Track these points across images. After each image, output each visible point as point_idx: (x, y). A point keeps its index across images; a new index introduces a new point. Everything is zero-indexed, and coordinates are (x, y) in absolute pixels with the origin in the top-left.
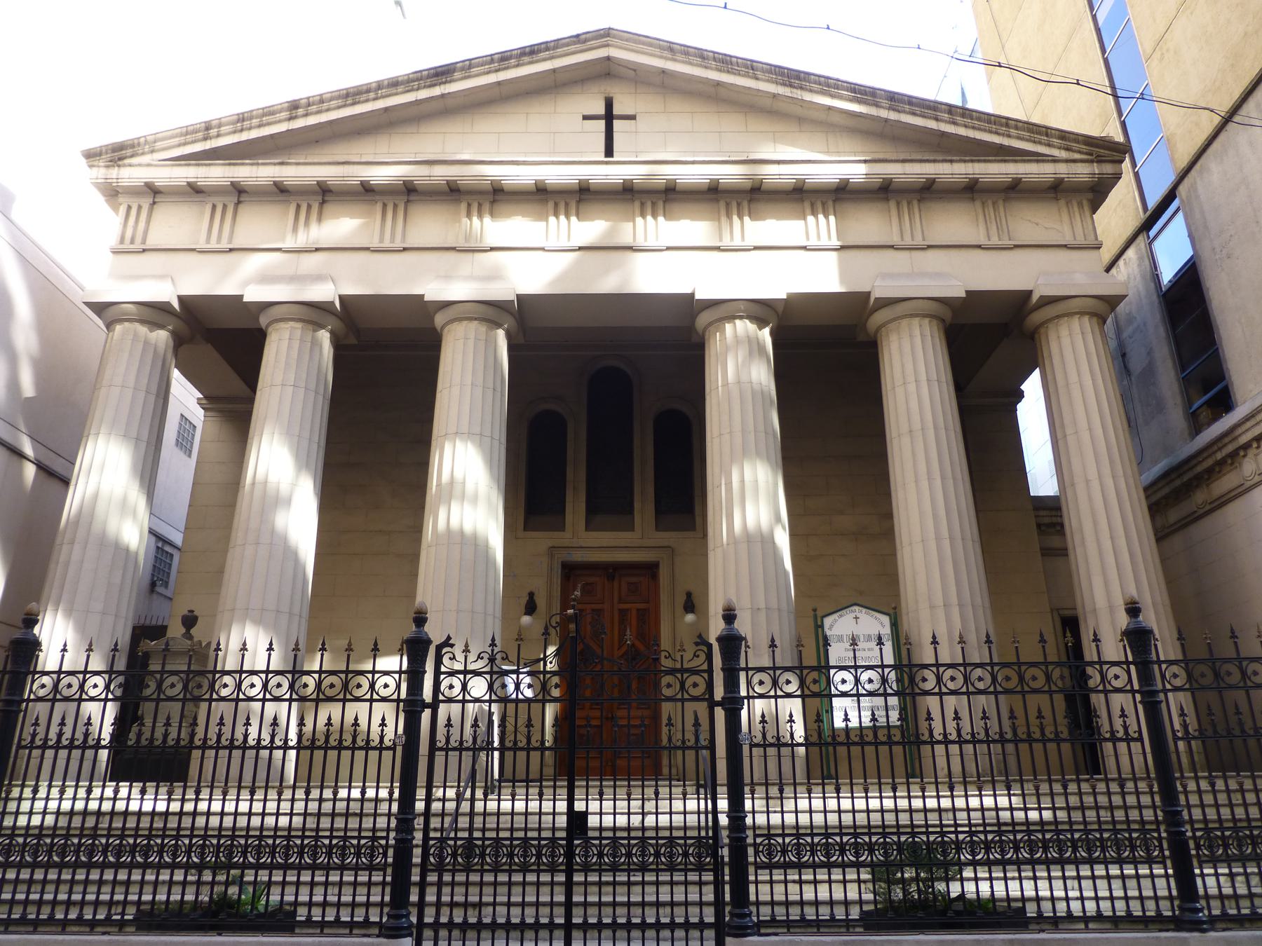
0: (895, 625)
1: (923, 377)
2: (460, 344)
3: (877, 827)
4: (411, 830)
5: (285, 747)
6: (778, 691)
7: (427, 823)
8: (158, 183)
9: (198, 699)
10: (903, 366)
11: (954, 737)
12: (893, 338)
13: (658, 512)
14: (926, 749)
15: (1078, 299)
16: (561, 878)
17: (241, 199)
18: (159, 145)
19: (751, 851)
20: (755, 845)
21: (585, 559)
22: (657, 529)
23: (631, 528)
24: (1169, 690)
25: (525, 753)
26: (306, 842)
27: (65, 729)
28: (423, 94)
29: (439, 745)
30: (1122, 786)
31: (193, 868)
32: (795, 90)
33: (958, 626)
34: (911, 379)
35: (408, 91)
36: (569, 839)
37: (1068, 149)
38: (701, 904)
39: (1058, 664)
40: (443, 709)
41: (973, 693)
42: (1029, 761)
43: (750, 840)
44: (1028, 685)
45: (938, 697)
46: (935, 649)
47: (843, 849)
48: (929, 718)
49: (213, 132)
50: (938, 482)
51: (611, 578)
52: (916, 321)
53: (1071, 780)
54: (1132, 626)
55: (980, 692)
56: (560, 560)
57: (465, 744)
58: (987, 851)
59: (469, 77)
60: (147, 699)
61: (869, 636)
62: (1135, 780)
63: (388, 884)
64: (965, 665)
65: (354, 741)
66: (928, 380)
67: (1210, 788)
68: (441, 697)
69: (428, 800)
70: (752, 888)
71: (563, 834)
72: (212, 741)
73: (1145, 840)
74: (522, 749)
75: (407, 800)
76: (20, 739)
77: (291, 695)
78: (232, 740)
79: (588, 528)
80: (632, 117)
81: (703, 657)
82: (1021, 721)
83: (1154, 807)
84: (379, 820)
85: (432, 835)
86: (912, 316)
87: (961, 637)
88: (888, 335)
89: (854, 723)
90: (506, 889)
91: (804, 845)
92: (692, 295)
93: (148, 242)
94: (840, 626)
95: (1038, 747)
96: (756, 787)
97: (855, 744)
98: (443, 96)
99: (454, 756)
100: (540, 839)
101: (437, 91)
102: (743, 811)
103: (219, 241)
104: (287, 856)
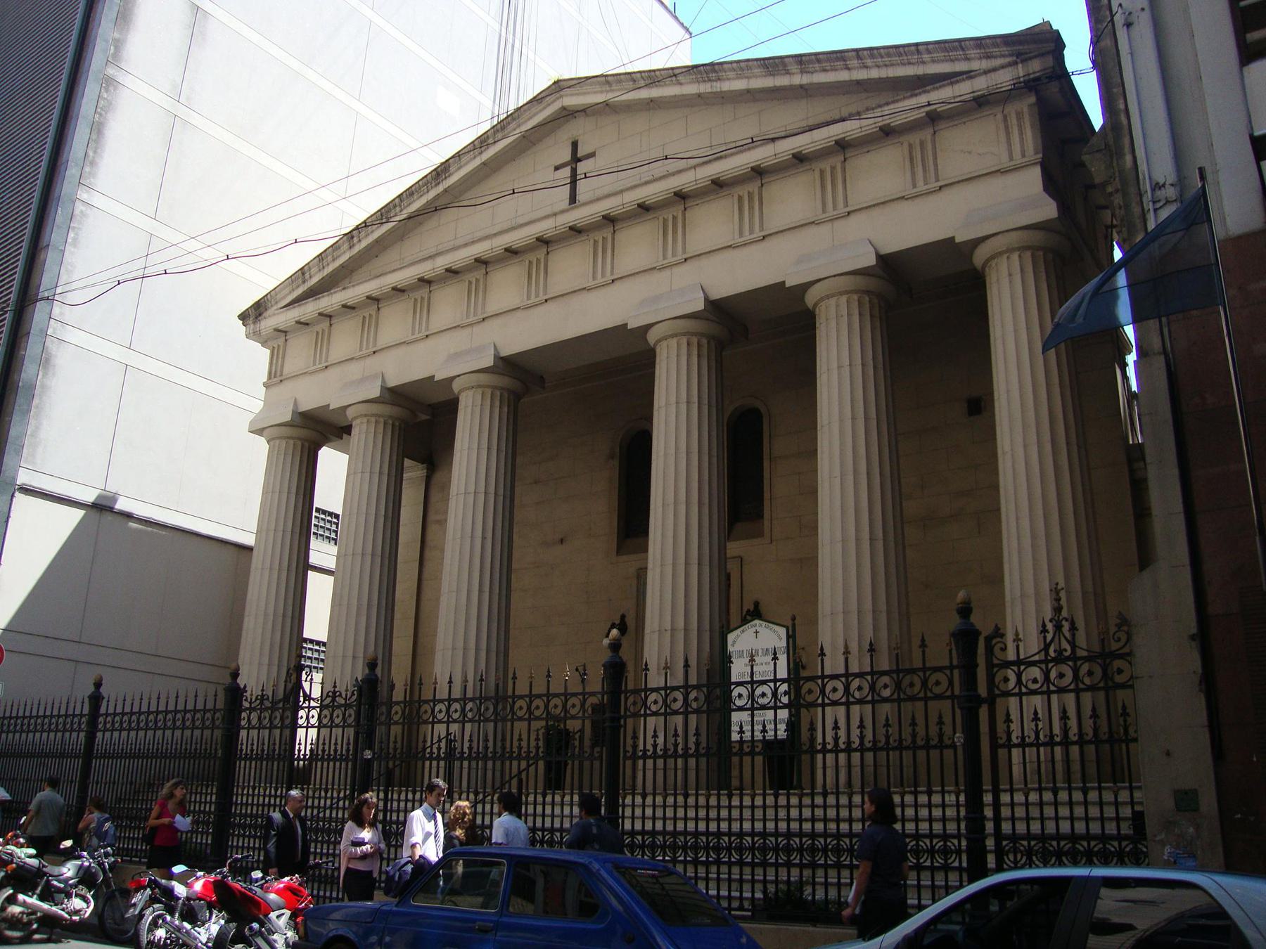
0: (791, 637)
2: (1005, 282)
5: (645, 757)
8: (328, 311)
9: (504, 720)
15: (999, 237)
17: (847, 156)
18: (279, 297)
24: (1054, 692)
27: (918, 729)
28: (432, 194)
32: (715, 84)
33: (869, 633)
35: (421, 196)
37: (989, 57)
39: (783, 681)
41: (1026, 694)
42: (750, 772)
48: (1008, 720)
49: (307, 276)
50: (695, 509)
53: (1093, 788)
55: (886, 700)
57: (904, 743)
59: (461, 167)
61: (767, 650)
62: (837, 794)
64: (752, 682)
65: (914, 741)
69: (997, 805)
72: (908, 741)
75: (975, 804)
76: (625, 752)
77: (873, 697)
78: (901, 740)
80: (592, 155)
82: (1073, 723)
83: (958, 820)
87: (871, 644)
89: (770, 735)
92: (953, 238)
93: (850, 202)
94: (744, 641)
98: (446, 191)
101: (441, 188)
103: (751, 232)
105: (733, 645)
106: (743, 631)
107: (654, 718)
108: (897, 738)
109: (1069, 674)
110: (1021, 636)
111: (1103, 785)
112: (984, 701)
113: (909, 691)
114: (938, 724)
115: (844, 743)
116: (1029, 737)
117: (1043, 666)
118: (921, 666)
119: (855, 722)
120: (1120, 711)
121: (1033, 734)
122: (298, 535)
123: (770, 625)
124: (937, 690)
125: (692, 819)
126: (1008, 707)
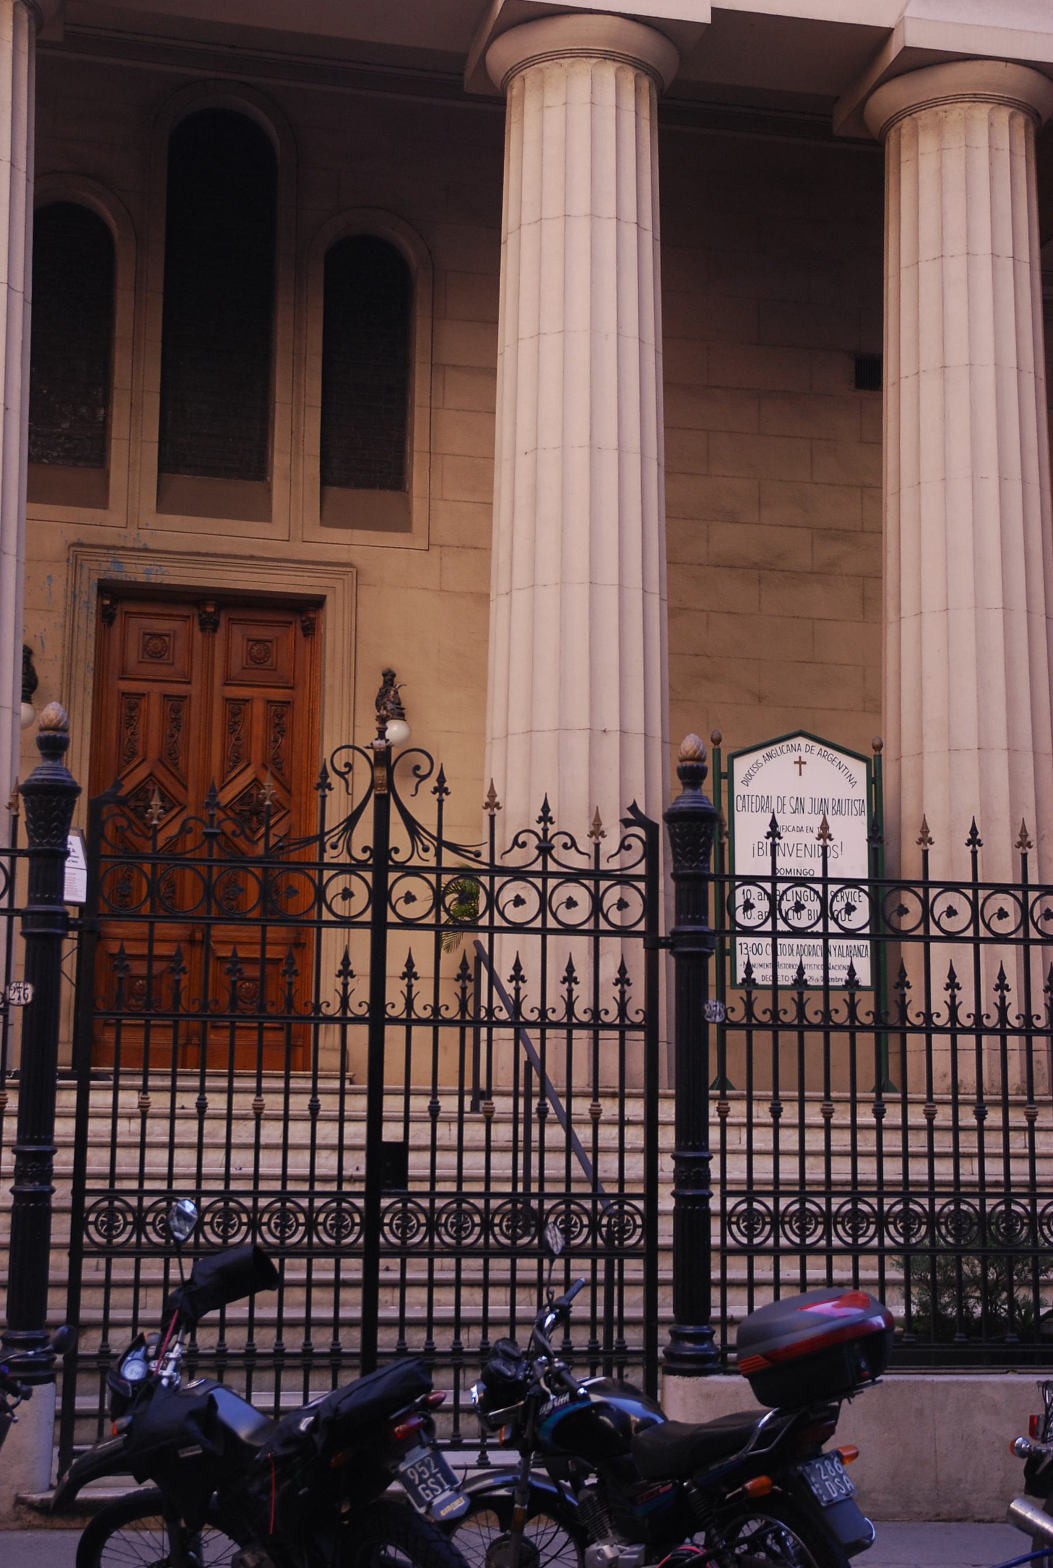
1: (983, 247)
3: (996, 1184)
4: (46, 1175)
6: (831, 924)
7: (80, 1161)
10: (942, 214)
11: (612, 1017)
12: (927, 144)
13: (326, 480)
14: (915, 1042)
16: (353, 1269)
19: (715, 1226)
20: (724, 1214)
21: (154, 579)
22: (326, 519)
23: (264, 514)
24: (1036, 942)
25: (795, 1034)
26: (783, 1203)
29: (391, 1012)
30: (981, 1115)
31: (442, 1255)
34: (956, 246)
36: (372, 1196)
38: (336, 1323)
40: (397, 942)
41: (986, 940)
43: (714, 1205)
44: (988, 926)
45: (921, 945)
46: (974, 853)
47: (777, 1220)
51: (209, 625)
52: (982, 112)
54: (685, 804)
56: (95, 577)
58: (775, 1232)
60: (907, 936)
62: (1005, 1105)
63: (716, 1285)
64: (975, 886)
66: (994, 255)
67: (771, 1120)
68: (391, 918)
70: (715, 1295)
71: (360, 1187)
72: (558, 1015)
73: (284, 1214)
74: (557, 1025)
78: (928, 1015)
79: (163, 507)
81: (638, 846)
84: (151, 1155)
85: (90, 1185)
86: (977, 98)
88: (915, 136)
90: (128, 1295)
91: (631, 1215)
95: (941, 1041)
96: (836, 1106)
97: (762, 1026)
99: (422, 1035)
100: (487, 1195)
102: (706, 1148)
104: (110, 1230)
105: (746, 782)
106: (770, 756)
107: (616, 941)
108: (591, 1006)
109: (533, 901)
110: (1032, 837)
111: (884, 1095)
112: (665, 943)
113: (615, 917)
114: (340, 974)
115: (1018, 1018)
116: (554, 1011)
117: (1019, 894)
118: (970, 880)
119: (609, 971)
120: (741, 975)
121: (338, 999)
122: (1006, 154)
123: (830, 751)
124: (515, 915)
125: (917, 1155)
126: (902, 965)
